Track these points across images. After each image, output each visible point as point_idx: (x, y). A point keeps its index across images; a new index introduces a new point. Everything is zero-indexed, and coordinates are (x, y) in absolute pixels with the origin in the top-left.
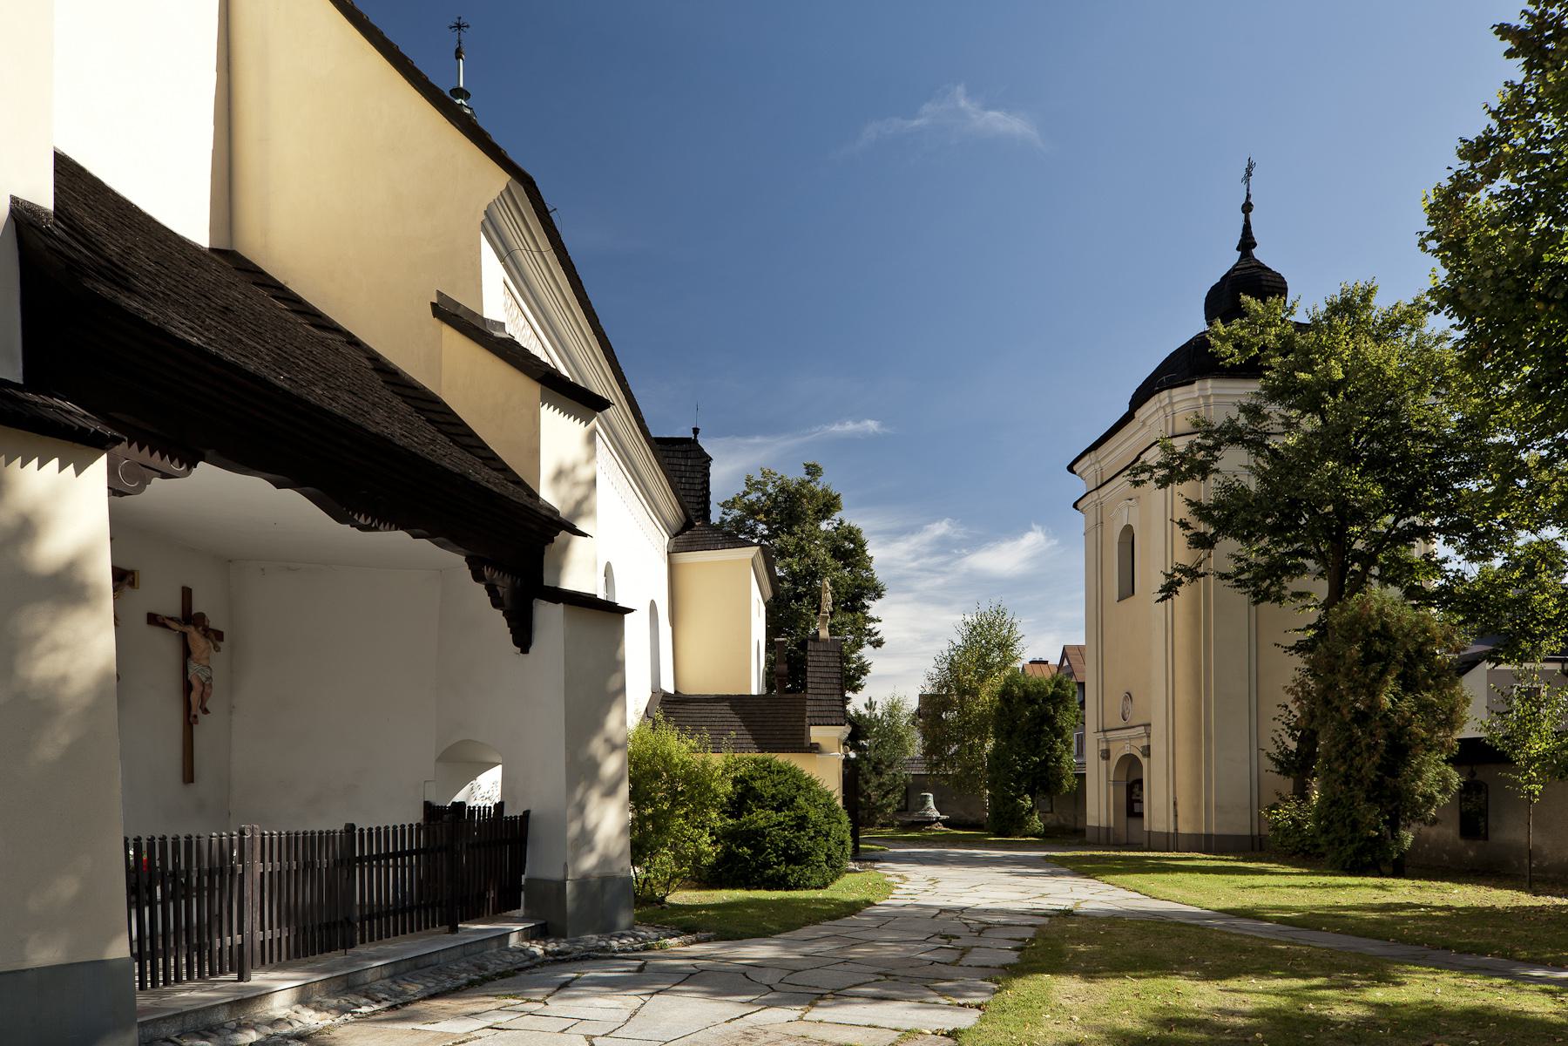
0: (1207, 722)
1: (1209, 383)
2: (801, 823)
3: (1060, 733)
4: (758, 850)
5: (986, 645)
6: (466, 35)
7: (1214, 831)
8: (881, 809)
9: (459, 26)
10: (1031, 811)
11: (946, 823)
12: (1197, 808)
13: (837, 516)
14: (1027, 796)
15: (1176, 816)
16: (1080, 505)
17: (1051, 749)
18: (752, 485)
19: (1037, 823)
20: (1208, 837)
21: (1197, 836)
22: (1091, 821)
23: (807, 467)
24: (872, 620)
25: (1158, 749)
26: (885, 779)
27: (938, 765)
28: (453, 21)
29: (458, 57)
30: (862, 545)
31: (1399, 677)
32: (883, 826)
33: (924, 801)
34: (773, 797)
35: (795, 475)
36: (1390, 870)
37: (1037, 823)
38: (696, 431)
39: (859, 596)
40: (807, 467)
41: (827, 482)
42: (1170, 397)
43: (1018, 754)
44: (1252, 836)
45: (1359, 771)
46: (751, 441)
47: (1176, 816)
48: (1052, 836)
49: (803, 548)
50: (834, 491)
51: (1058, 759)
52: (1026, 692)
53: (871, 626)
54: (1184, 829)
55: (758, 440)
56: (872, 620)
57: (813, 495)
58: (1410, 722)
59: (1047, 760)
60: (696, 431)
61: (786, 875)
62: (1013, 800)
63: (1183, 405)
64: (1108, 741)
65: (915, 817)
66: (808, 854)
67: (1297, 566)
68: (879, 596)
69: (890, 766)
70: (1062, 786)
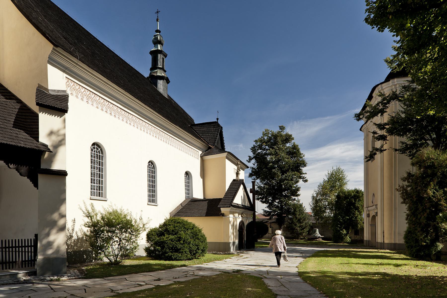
0: (395, 203)
1: (396, 80)
2: (179, 239)
3: (357, 208)
4: (163, 248)
5: (335, 179)
6: (159, 14)
7: (397, 242)
8: (301, 234)
9: (158, 12)
10: (346, 235)
11: (323, 239)
12: (391, 234)
13: (293, 141)
14: (344, 230)
15: (384, 237)
16: (362, 129)
17: (354, 214)
18: (264, 134)
19: (348, 239)
20: (395, 244)
21: (391, 244)
22: (365, 239)
23: (280, 127)
24: (304, 174)
25: (379, 214)
26: (303, 224)
27: (318, 219)
28: (156, 11)
29: (157, 21)
30: (298, 150)
31: (438, 183)
32: (302, 239)
33: (315, 231)
34: (173, 231)
35: (276, 130)
36: (434, 258)
37: (348, 239)
38: (218, 119)
39: (299, 167)
40: (280, 127)
41: (288, 131)
42: (382, 87)
43: (341, 216)
44: (381, 243)
45: (419, 219)
46: (326, 118)
47: (384, 237)
48: (354, 243)
49: (277, 153)
50: (290, 133)
51: (356, 217)
52: (345, 195)
53: (303, 175)
54: (386, 241)
55: (328, 118)
56: (304, 174)
57: (281, 136)
58: (440, 200)
59: (352, 217)
60: (218, 119)
61: (171, 256)
62: (339, 231)
63: (387, 89)
64: (369, 211)
65: (312, 236)
66: (180, 249)
67: (423, 144)
68: (305, 166)
69: (304, 220)
70: (357, 227)
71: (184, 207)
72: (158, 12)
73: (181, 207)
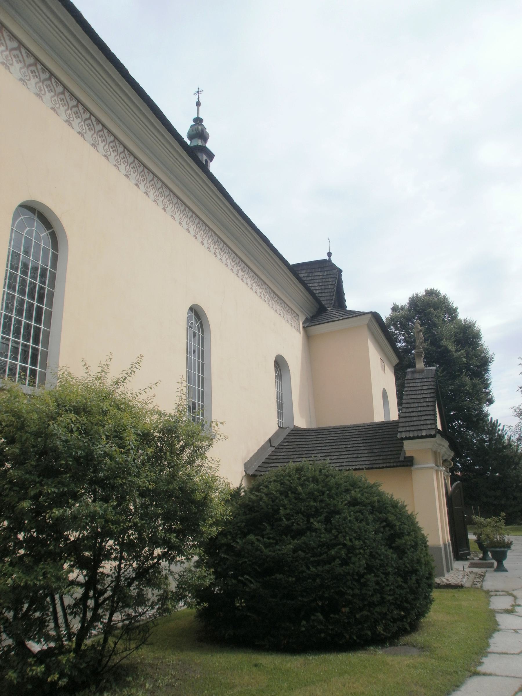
9: (198, 92)
71: (278, 449)
72: (198, 92)
73: (270, 450)
